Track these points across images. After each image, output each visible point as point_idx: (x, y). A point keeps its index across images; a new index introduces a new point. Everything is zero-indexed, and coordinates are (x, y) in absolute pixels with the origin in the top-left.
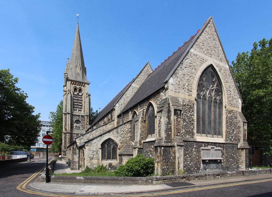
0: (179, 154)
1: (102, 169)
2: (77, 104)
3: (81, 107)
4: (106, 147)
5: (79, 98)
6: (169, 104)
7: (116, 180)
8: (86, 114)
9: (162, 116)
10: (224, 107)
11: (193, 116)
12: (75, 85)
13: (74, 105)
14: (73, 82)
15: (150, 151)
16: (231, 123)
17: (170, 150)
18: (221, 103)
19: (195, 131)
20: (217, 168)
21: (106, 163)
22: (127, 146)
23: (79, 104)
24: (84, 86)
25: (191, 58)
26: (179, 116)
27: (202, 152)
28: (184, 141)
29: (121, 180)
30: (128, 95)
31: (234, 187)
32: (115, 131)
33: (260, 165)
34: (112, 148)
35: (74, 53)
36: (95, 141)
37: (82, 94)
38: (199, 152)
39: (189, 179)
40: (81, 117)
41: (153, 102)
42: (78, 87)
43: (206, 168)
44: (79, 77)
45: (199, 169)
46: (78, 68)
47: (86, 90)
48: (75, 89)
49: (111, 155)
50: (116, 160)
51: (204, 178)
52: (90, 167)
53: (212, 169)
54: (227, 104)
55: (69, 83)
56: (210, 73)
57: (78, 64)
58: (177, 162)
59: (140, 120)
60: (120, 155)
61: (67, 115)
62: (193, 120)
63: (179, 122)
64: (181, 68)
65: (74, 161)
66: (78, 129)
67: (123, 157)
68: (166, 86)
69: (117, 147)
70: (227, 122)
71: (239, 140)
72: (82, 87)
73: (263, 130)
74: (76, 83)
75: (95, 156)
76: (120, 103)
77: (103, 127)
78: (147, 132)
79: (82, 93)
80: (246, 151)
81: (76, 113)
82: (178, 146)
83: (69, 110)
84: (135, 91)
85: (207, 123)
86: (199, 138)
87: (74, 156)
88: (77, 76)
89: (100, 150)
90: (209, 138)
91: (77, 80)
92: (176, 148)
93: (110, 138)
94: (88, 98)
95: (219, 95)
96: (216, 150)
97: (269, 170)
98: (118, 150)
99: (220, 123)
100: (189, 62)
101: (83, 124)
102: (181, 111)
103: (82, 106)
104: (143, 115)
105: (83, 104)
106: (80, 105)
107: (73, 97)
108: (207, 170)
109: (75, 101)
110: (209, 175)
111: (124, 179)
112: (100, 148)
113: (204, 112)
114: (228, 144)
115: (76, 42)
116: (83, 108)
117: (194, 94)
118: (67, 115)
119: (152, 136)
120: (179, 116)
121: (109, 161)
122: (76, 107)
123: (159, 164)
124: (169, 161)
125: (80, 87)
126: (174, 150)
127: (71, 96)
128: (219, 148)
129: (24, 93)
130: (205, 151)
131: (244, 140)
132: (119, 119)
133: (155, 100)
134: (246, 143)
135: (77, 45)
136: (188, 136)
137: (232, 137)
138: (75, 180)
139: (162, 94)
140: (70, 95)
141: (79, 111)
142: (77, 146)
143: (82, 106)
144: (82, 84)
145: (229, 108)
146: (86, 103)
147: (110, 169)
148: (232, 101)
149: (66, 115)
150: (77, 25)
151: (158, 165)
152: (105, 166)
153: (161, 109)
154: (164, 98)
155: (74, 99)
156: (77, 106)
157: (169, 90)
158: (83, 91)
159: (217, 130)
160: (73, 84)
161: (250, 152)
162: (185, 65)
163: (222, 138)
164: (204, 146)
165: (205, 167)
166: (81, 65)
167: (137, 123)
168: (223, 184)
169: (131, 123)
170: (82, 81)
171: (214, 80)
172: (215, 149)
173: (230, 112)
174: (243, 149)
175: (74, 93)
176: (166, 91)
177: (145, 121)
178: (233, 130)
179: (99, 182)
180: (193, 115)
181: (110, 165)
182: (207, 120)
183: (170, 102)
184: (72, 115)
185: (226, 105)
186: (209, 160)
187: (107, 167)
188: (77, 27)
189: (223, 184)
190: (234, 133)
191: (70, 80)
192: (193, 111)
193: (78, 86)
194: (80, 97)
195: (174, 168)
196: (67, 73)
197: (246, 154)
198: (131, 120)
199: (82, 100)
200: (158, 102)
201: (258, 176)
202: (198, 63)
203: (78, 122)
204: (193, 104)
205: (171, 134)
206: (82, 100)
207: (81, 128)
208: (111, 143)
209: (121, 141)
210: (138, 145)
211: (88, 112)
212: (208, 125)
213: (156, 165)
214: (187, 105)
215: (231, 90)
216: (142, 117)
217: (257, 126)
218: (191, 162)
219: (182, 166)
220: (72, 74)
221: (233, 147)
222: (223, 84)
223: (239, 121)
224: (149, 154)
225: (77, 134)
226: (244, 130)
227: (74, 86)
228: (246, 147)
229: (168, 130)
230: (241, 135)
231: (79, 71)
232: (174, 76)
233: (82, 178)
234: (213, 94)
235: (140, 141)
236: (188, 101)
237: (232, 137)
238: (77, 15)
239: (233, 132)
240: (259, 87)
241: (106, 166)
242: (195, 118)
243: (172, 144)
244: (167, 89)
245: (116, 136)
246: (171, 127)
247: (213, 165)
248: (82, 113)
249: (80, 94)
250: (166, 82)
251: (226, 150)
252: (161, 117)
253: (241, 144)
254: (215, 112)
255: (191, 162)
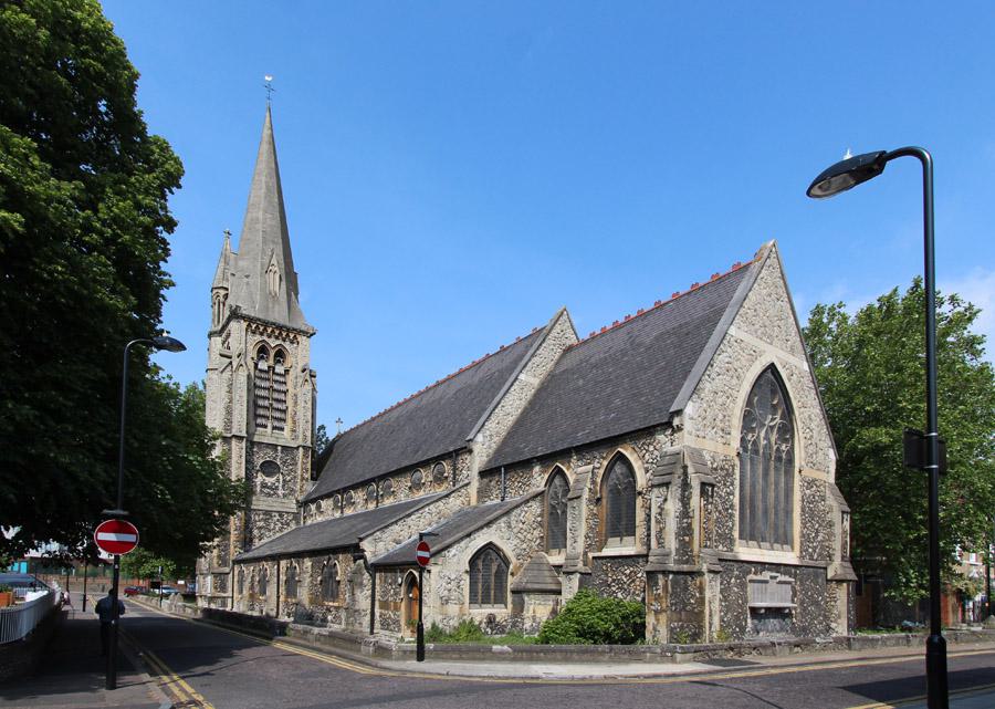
0: (712, 590)
1: (471, 629)
2: (266, 403)
3: (283, 416)
4: (481, 567)
5: (276, 381)
6: (685, 467)
7: (591, 651)
8: (300, 442)
9: (669, 497)
10: (797, 470)
11: (731, 497)
12: (262, 334)
13: (257, 406)
14: (254, 326)
15: (618, 582)
16: (810, 514)
17: (686, 582)
18: (790, 461)
19: (736, 534)
20: (782, 630)
21: (479, 614)
22: (536, 567)
23: (275, 405)
24: (292, 342)
25: (729, 349)
26: (710, 500)
27: (750, 587)
28: (720, 560)
29: (604, 652)
30: (508, 409)
31: (847, 668)
32: (502, 523)
33: (874, 627)
34: (494, 571)
35: (258, 219)
36: (453, 551)
37: (287, 371)
38: (743, 586)
39: (740, 653)
40: (282, 452)
41: (631, 453)
42: (273, 342)
43: (759, 628)
44: (277, 307)
45: (743, 630)
46: (272, 274)
47: (300, 354)
48: (263, 351)
49: (492, 592)
50: (503, 606)
51: (769, 651)
52: (441, 626)
53: (771, 632)
54: (803, 463)
55: (237, 328)
56: (771, 380)
57: (274, 261)
58: (707, 612)
59: (586, 495)
60: (513, 592)
61: (234, 442)
62: (732, 506)
63: (709, 513)
64: (709, 376)
65: (357, 608)
66: (269, 495)
67: (526, 598)
68: (676, 422)
69: (508, 567)
70: (803, 510)
71: (830, 556)
72: (287, 345)
73: (887, 530)
74: (265, 329)
75: (454, 595)
76: (488, 432)
77: (437, 504)
78: (604, 529)
79: (287, 365)
80: (848, 586)
81: (265, 435)
82: (710, 571)
83: (240, 425)
84: (529, 397)
85: (760, 513)
86: (746, 552)
87: (358, 592)
88: (271, 305)
89: (467, 577)
90: (765, 551)
91: (271, 319)
92: (707, 577)
93: (491, 543)
94: (308, 387)
95: (786, 441)
96: (780, 582)
97: (903, 638)
98: (510, 577)
99: (789, 513)
100: (727, 360)
101: (289, 478)
102: (713, 486)
103: (284, 411)
104: (594, 482)
105: (290, 403)
106: (278, 410)
107: (255, 376)
108: (761, 634)
109: (263, 393)
110: (780, 644)
111: (611, 650)
112: (467, 572)
113: (753, 486)
114: (806, 567)
115: (263, 179)
116: (289, 421)
117: (736, 444)
118: (234, 442)
119: (624, 541)
120: (710, 500)
121: (487, 610)
122: (263, 416)
123: (663, 618)
124: (684, 608)
125: (278, 342)
126: (701, 583)
127: (249, 376)
128: (787, 578)
129: (173, 381)
130: (756, 585)
131: (843, 558)
132: (485, 480)
133: (637, 449)
134: (848, 564)
135: (267, 187)
136: (721, 547)
137: (814, 549)
138: (489, 654)
139: (660, 437)
140: (246, 373)
141: (274, 428)
142: (366, 562)
143: (284, 411)
144: (287, 335)
145: (810, 474)
146: (301, 404)
147: (489, 630)
148: (815, 454)
149: (230, 444)
150: (268, 114)
151: (658, 620)
152: (477, 623)
153: (666, 479)
154: (668, 448)
155: (256, 386)
156: (267, 413)
157: (685, 430)
158: (290, 360)
159: (781, 531)
160: (254, 332)
161: (858, 589)
162: (717, 369)
163: (793, 548)
164: (755, 573)
165: (756, 626)
166: (283, 266)
167: (575, 503)
168: (811, 664)
169: (542, 501)
170: (288, 324)
171: (775, 402)
172: (778, 580)
173: (810, 483)
174: (840, 582)
175: (256, 365)
176: (674, 432)
177: (599, 500)
178: (817, 532)
179: (549, 657)
180: (733, 494)
181: (491, 620)
182: (759, 505)
183: (688, 463)
184: (251, 444)
185: (802, 466)
186: (767, 609)
187: (483, 625)
188: (268, 124)
189: (811, 664)
190: (819, 538)
191: (244, 318)
192: (732, 484)
193: (273, 339)
194: (277, 378)
195: (701, 627)
196: (227, 289)
197: (848, 594)
198: (543, 492)
199: (285, 393)
200: (647, 457)
201: (880, 651)
202: (744, 363)
203: (269, 468)
204: (733, 466)
205: (691, 542)
206: (285, 393)
207: (280, 492)
208: (494, 556)
209: (519, 551)
210: (580, 566)
211: (309, 434)
212: (764, 521)
213: (650, 620)
214: (722, 469)
215: (813, 426)
216: (590, 489)
217: (868, 519)
218: (727, 611)
219: (716, 620)
220: (251, 294)
221: (817, 576)
222: (796, 413)
223: (831, 507)
224: (614, 589)
225: (267, 513)
226: (844, 532)
227: (258, 338)
228: (849, 577)
229: (685, 531)
230: (837, 545)
231: (275, 284)
232: (695, 396)
233: (506, 647)
234: (774, 437)
235: (585, 554)
236: (722, 457)
237: (814, 549)
238: (267, 78)
239: (817, 536)
240: (875, 419)
241: (481, 623)
242: (736, 500)
243: (695, 568)
244: (679, 429)
245: (506, 535)
246: (690, 525)
247: (773, 622)
248: (285, 437)
249: (280, 369)
250: (679, 412)
251: (801, 582)
252: (666, 500)
253: (837, 567)
254: (777, 484)
255: (727, 611)
